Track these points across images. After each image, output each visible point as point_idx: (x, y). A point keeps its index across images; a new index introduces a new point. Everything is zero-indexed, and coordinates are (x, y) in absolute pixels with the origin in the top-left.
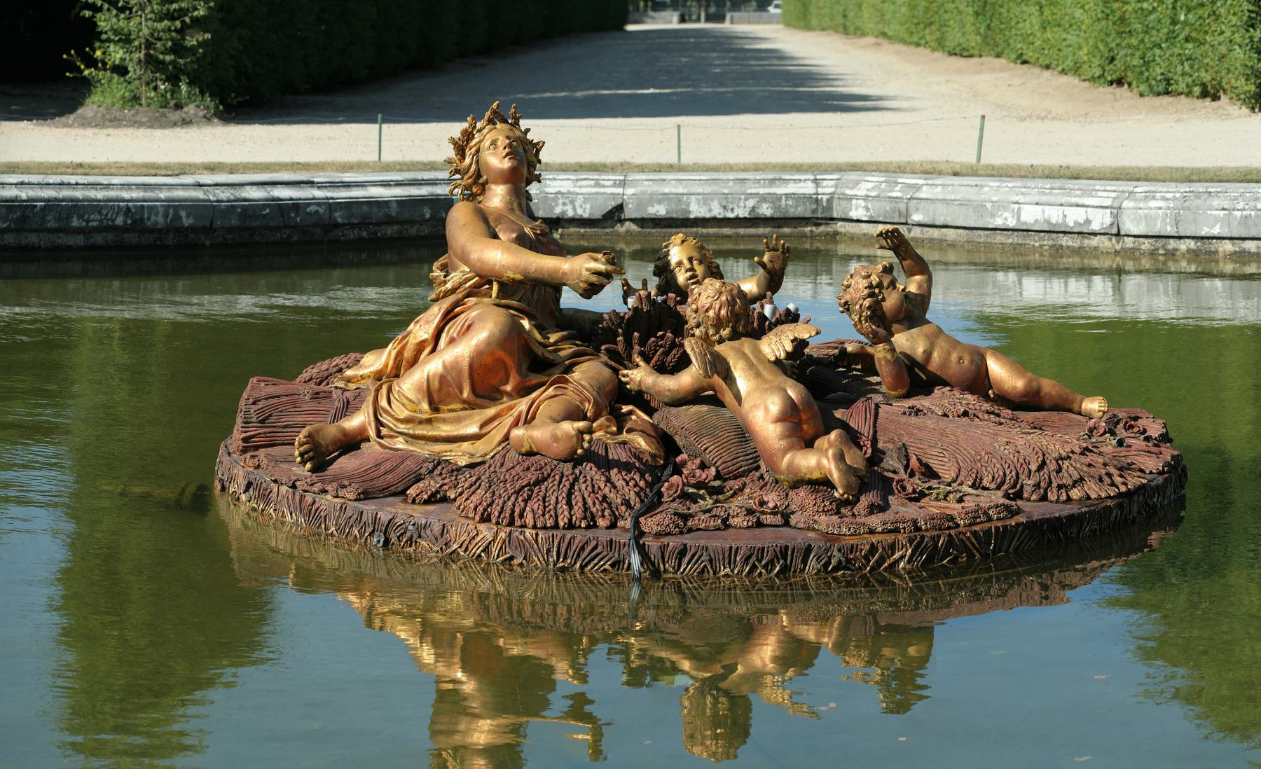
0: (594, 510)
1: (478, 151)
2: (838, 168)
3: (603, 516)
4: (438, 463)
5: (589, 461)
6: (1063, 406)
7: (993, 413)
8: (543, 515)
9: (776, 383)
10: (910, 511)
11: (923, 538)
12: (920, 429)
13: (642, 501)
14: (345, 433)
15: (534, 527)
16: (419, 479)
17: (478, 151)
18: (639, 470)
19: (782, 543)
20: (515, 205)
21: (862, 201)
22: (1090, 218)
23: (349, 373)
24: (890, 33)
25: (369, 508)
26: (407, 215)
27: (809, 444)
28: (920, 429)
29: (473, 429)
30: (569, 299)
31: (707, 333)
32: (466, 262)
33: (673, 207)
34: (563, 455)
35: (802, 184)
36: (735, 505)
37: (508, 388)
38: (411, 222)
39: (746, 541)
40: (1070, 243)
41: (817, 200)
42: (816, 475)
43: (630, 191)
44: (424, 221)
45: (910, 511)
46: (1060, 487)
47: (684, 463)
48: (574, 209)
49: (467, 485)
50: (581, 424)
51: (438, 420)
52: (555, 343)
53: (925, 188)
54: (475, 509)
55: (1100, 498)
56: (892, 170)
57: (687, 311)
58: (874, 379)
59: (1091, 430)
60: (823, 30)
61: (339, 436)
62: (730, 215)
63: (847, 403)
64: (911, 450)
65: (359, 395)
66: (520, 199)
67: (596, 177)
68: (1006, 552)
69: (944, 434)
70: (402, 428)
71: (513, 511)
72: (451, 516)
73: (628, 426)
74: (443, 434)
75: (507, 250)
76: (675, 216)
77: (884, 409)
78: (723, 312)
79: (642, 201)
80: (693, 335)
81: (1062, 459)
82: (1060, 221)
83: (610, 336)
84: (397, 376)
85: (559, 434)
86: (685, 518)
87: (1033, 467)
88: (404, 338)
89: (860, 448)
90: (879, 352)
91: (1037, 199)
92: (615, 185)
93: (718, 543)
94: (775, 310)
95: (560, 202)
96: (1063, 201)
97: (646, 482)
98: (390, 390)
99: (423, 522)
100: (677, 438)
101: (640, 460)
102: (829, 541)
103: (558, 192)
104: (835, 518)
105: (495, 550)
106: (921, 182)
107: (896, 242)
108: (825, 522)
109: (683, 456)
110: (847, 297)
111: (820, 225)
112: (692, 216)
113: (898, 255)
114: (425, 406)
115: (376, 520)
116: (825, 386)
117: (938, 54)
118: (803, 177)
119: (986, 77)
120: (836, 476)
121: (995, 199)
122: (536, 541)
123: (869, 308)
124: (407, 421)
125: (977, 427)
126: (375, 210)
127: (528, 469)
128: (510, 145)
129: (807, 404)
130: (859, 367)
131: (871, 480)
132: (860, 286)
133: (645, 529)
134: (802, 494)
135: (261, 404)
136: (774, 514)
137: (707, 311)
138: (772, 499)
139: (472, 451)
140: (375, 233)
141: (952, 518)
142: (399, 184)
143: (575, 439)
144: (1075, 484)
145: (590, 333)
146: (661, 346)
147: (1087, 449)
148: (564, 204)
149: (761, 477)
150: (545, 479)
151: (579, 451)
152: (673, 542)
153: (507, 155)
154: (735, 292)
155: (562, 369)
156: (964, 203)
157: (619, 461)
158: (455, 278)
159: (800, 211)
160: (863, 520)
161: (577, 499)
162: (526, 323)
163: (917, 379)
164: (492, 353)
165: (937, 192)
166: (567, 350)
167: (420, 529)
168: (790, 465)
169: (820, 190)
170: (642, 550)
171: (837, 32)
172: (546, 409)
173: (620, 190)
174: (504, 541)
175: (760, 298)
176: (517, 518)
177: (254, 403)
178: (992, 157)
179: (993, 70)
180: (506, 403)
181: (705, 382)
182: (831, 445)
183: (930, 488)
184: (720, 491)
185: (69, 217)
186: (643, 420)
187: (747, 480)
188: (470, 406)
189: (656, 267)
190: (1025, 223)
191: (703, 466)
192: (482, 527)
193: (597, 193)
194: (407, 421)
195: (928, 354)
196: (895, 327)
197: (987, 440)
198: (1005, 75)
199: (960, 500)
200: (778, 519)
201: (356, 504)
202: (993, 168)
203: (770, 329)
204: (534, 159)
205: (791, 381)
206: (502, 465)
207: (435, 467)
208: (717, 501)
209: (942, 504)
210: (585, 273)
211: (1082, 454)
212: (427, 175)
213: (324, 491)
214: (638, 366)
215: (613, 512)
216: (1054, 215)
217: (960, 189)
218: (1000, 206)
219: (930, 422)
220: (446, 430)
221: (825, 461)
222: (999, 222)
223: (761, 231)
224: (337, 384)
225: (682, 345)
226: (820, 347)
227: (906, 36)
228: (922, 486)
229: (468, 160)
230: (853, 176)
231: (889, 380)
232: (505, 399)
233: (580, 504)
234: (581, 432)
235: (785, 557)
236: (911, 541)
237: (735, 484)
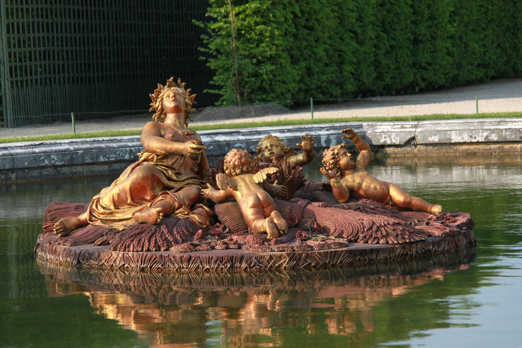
1: (162, 100)
3: (163, 246)
4: (111, 230)
8: (137, 246)
11: (294, 254)
19: (231, 255)
29: (130, 216)
31: (230, 171)
33: (442, 137)
35: (516, 123)
48: (391, 140)
61: (78, 223)
62: (474, 140)
74: (117, 218)
92: (412, 127)
95: (383, 136)
120: (268, 230)
122: (133, 257)
123: (332, 164)
135: (52, 213)
137: (230, 162)
139: (126, 224)
142: (289, 131)
148: (385, 137)
173: (414, 130)
177: (49, 212)
185: (98, 157)
186: (206, 211)
193: (401, 132)
195: (360, 185)
210: (189, 149)
213: (59, 244)
235: (232, 261)
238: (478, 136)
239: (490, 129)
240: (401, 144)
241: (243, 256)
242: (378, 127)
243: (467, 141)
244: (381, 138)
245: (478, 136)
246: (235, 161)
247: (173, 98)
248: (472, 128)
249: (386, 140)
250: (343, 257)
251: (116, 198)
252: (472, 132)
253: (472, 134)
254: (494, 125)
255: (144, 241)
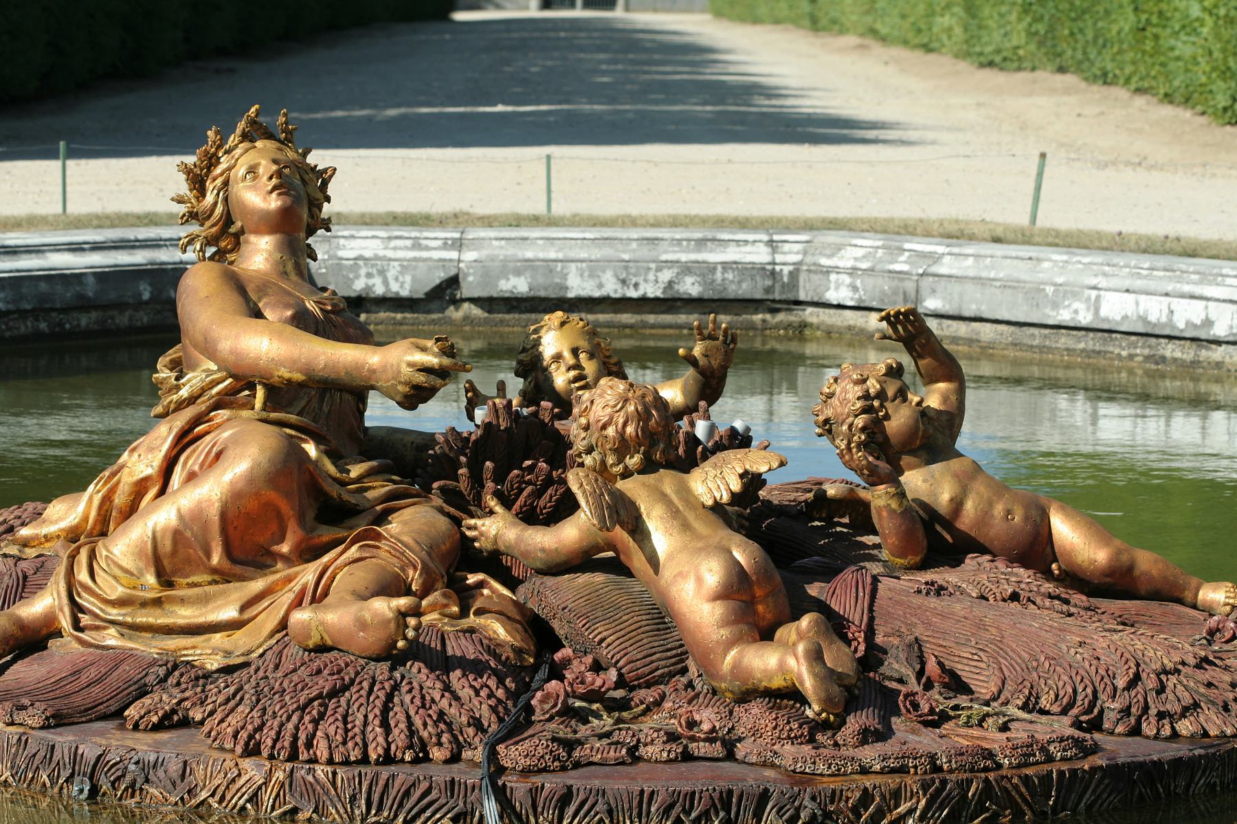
0: (425, 734)
1: (226, 183)
2: (808, 226)
3: (440, 744)
4: (174, 666)
5: (416, 658)
6: (1169, 594)
7: (1058, 598)
8: (344, 743)
9: (715, 540)
10: (926, 741)
11: (944, 782)
12: (943, 616)
13: (501, 720)
14: (21, 624)
15: (330, 762)
16: (143, 693)
17: (226, 183)
18: (495, 672)
19: (723, 785)
20: (290, 267)
21: (846, 276)
22: (1212, 317)
23: (25, 532)
24: (884, 31)
25: (63, 739)
26: (112, 295)
27: (766, 635)
28: (943, 616)
29: (229, 613)
30: (381, 413)
31: (603, 462)
32: (212, 354)
33: (541, 280)
34: (375, 649)
35: (749, 248)
36: (647, 726)
37: (285, 548)
38: (121, 306)
39: (666, 782)
40: (1178, 354)
41: (773, 273)
42: (777, 683)
43: (469, 256)
44: (140, 305)
45: (926, 741)
46: (1161, 715)
47: (567, 662)
48: (386, 282)
49: (221, 699)
50: (403, 602)
51: (172, 600)
52: (359, 479)
53: (947, 259)
54: (235, 736)
55: (1223, 735)
56: (896, 230)
57: (572, 428)
58: (869, 540)
59: (1212, 633)
60: (777, 21)
61: (13, 629)
62: (633, 294)
63: (828, 574)
64: (927, 648)
65: (43, 566)
66: (296, 253)
67: (414, 234)
68: (1074, 810)
69: (981, 626)
70: (114, 613)
71: (295, 738)
72: (195, 748)
73: (478, 604)
74: (181, 621)
75: (279, 335)
76: (542, 294)
77: (886, 584)
78: (630, 430)
79: (486, 270)
80: (582, 465)
81: (1166, 672)
82: (1164, 319)
83: (447, 467)
84: (104, 534)
85: (368, 616)
86: (570, 745)
87: (1121, 683)
88: (114, 474)
89: (848, 642)
90: (879, 498)
91: (1127, 283)
92: (445, 247)
93: (621, 784)
94: (712, 429)
95: (363, 272)
96: (1170, 288)
97: (507, 689)
98: (92, 556)
99: (152, 758)
100: (555, 624)
101: (497, 657)
102: (796, 783)
103: (356, 255)
104: (807, 749)
105: (267, 798)
106: (941, 249)
107: (909, 329)
108: (791, 755)
109: (566, 652)
110: (829, 412)
111: (777, 311)
112: (571, 295)
113: (910, 349)
114: (151, 579)
115: (75, 757)
116: (792, 545)
117: (963, 65)
118: (751, 237)
119: (1042, 101)
120: (808, 684)
121: (1060, 280)
122: (334, 784)
123: (863, 429)
124: (121, 603)
125: (1034, 617)
126: (59, 288)
127: (319, 672)
128: (279, 174)
129: (764, 575)
130: (846, 520)
131: (863, 690)
132: (850, 396)
133: (506, 763)
134: (755, 711)
136: (711, 740)
137: (604, 427)
138: (707, 718)
140: (61, 324)
141: (990, 755)
142: (97, 247)
143: (392, 626)
144: (1185, 712)
145: (412, 463)
146: (529, 483)
147: (1205, 660)
148: (369, 275)
149: (690, 685)
150: (345, 688)
151: (400, 644)
152: (551, 784)
153: (274, 188)
154: (649, 399)
155: (370, 518)
156: (1008, 285)
157: (463, 658)
158: (192, 381)
159: (745, 289)
160: (851, 752)
161: (397, 717)
162: (311, 449)
163: (938, 541)
164: (257, 495)
165: (967, 266)
166: (379, 489)
167: (147, 770)
168: (736, 666)
169: (779, 258)
170: (502, 795)
171: (801, 27)
172: (345, 580)
173: (454, 255)
174: (283, 785)
175: (689, 410)
176: (302, 749)
178: (1053, 217)
179: (1052, 91)
180: (281, 571)
181: (601, 537)
182: (801, 637)
183: (956, 708)
184: (624, 705)
186: (501, 596)
187: (668, 689)
188: (223, 577)
189: (520, 362)
190: (1106, 320)
191: (597, 667)
192: (247, 764)
193: (415, 259)
194: (121, 603)
195: (957, 504)
196: (906, 460)
197: (1050, 638)
198: (1073, 99)
199: (1004, 728)
200: (717, 750)
201: (42, 734)
202: (1057, 233)
203: (705, 458)
204: (320, 195)
205: (738, 538)
206: (277, 667)
207: (169, 673)
208: (619, 721)
209: (976, 732)
210: (406, 370)
211: (1198, 666)
212: (143, 233)
214: (491, 513)
215: (455, 737)
216: (1155, 310)
217: (1005, 263)
218: (1067, 292)
219: (958, 607)
220: (185, 615)
221: (792, 662)
222: (1064, 316)
223: (682, 318)
224: (7, 551)
225: (563, 482)
226: (784, 488)
227: (910, 35)
228: (943, 704)
229: (210, 198)
230: (832, 237)
231: (892, 540)
232: (280, 565)
233: (402, 726)
234: (402, 615)
235: (727, 807)
236: (925, 787)
237: (650, 695)
238: (646, 281)
239: (677, 262)
240: (415, 296)
241: (766, 790)
242: (342, 241)
243: (613, 295)
244: (357, 277)
245: (646, 281)
246: (625, 424)
247: (274, 181)
248: (626, 257)
249: (371, 282)
250: (1094, 791)
251: (166, 545)
252: (626, 268)
253: (628, 274)
254: (688, 251)
255: (365, 724)
